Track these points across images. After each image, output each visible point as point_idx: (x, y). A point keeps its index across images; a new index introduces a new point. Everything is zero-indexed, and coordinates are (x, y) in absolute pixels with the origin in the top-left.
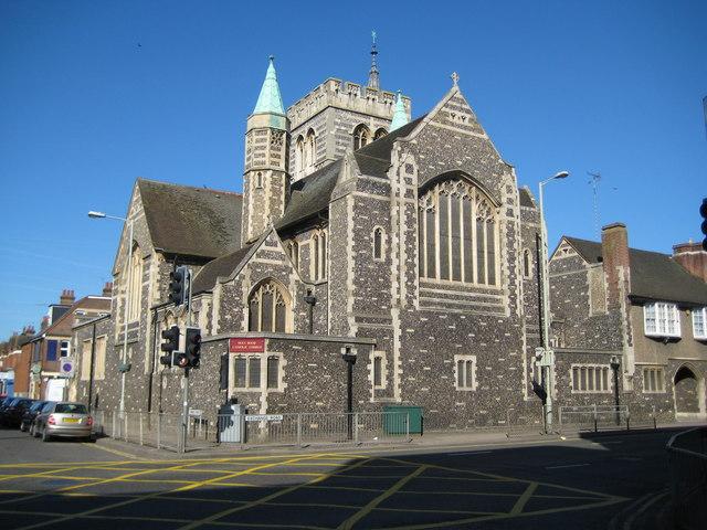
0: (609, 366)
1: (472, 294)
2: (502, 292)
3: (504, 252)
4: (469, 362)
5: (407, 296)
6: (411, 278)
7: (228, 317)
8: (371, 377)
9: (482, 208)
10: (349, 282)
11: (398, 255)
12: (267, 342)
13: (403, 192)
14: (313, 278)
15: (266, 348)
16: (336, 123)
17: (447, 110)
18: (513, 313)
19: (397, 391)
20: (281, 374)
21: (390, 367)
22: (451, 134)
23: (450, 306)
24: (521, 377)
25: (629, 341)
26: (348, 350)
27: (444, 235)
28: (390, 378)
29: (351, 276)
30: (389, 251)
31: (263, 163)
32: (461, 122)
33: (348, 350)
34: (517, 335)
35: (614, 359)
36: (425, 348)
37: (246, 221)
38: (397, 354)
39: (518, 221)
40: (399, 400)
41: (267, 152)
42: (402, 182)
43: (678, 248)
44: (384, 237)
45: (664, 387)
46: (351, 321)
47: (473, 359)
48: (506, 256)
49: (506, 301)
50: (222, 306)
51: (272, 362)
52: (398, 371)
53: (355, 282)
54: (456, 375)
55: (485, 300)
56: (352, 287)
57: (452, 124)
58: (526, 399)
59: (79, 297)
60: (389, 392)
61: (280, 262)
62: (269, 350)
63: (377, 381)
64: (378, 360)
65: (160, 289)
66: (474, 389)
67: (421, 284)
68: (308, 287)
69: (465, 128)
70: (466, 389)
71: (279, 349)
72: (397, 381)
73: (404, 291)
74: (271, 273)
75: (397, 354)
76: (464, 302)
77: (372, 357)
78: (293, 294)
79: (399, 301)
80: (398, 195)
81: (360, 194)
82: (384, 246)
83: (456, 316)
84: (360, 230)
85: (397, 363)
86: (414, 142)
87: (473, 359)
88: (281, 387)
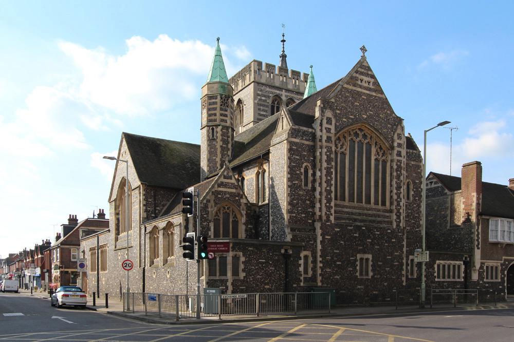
0: (462, 263)
4: (367, 260)
5: (326, 213)
6: (329, 201)
8: (301, 269)
9: (379, 150)
12: (231, 245)
13: (324, 138)
15: (231, 249)
16: (258, 95)
17: (357, 75)
18: (398, 225)
19: (319, 278)
20: (242, 266)
23: (355, 220)
24: (402, 269)
28: (314, 269)
30: (314, 181)
31: (215, 120)
32: (366, 85)
33: (286, 250)
34: (400, 240)
35: (466, 258)
38: (319, 253)
39: (404, 160)
40: (320, 284)
41: (218, 112)
42: (324, 131)
44: (310, 172)
45: (499, 277)
46: (287, 230)
47: (370, 256)
48: (395, 185)
51: (236, 259)
54: (358, 268)
55: (379, 216)
57: (361, 87)
58: (404, 284)
59: (81, 219)
61: (234, 191)
62: (233, 251)
67: (336, 205)
69: (369, 89)
71: (240, 249)
72: (319, 271)
73: (324, 209)
75: (319, 253)
77: (302, 255)
78: (244, 213)
79: (320, 216)
80: (321, 140)
82: (310, 178)
83: (359, 227)
86: (333, 100)
87: (370, 256)
88: (242, 275)
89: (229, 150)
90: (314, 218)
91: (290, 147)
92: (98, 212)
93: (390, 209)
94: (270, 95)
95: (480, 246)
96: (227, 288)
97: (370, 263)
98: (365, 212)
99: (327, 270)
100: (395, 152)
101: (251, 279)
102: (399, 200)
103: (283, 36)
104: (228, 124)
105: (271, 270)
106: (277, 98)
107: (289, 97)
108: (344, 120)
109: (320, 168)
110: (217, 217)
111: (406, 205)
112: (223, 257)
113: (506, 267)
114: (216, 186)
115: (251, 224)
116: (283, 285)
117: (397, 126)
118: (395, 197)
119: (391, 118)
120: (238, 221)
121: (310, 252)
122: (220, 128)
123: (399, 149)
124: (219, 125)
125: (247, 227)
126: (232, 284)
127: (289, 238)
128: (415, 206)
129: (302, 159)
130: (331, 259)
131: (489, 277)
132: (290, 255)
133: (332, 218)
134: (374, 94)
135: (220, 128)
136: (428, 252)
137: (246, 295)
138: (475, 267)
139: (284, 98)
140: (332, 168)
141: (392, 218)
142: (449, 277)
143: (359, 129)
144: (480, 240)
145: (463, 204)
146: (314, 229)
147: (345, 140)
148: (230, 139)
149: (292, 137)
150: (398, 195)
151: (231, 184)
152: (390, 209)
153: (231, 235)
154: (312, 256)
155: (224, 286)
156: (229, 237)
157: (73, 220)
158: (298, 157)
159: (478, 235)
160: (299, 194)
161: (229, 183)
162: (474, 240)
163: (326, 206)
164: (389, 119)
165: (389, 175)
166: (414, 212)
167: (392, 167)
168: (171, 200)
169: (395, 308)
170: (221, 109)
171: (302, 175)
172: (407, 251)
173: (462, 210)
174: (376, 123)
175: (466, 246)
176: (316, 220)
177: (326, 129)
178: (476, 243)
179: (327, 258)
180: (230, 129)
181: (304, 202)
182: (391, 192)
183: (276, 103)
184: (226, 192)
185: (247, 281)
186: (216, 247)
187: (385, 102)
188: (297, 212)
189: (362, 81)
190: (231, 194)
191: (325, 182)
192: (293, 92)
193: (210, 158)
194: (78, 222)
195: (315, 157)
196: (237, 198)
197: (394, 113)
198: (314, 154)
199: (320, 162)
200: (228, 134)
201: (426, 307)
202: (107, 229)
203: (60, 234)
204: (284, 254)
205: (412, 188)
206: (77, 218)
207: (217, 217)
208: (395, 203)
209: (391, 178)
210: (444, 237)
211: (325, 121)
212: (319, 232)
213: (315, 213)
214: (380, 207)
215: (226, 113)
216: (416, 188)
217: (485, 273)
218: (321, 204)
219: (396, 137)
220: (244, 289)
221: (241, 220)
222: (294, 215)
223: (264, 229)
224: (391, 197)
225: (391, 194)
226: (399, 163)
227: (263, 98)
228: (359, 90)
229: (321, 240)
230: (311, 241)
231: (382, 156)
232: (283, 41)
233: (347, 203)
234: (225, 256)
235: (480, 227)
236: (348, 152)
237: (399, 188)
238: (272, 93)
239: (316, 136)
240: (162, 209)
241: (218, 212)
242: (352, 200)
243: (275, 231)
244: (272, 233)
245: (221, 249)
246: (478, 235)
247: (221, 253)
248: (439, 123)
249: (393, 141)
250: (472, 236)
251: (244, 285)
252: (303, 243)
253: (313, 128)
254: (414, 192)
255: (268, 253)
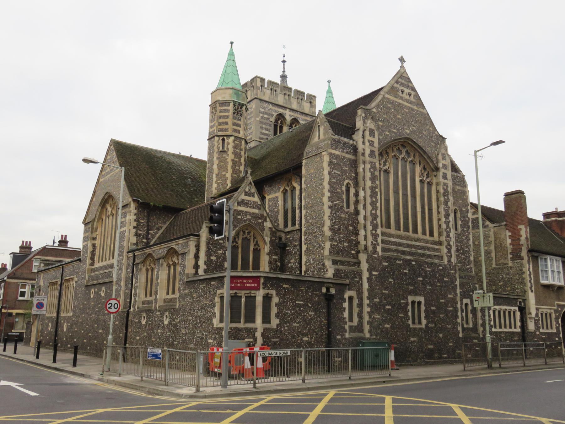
0: (517, 308)
1: (418, 244)
2: (440, 243)
3: (442, 209)
4: (419, 303)
5: (372, 243)
6: (375, 227)
7: (213, 258)
8: (346, 314)
9: (423, 171)
10: (326, 229)
11: (365, 206)
12: (262, 281)
13: (367, 152)
14: (281, 226)
15: (261, 286)
16: (260, 112)
17: (398, 86)
18: (449, 261)
19: (367, 328)
20: (274, 310)
21: (360, 305)
22: (401, 106)
23: (404, 253)
24: (457, 316)
25: (531, 288)
26: (328, 289)
27: (396, 192)
28: (360, 315)
29: (328, 223)
30: (357, 202)
31: (227, 130)
32: (407, 97)
33: (328, 289)
34: (453, 280)
35: (520, 302)
36: (386, 289)
37: (211, 180)
38: (366, 294)
39: (450, 183)
40: (368, 335)
41: (230, 121)
42: (367, 144)
43: (546, 215)
44: (352, 191)
45: (554, 327)
46: (328, 263)
47: (422, 299)
48: (443, 213)
49: (444, 250)
50: (208, 248)
51: (267, 299)
52: (367, 309)
53: (331, 229)
54: (410, 314)
55: (428, 249)
56: (328, 233)
57: (402, 98)
58: (461, 335)
59: (36, 247)
60: (359, 328)
61: (256, 211)
62: (264, 288)
63: (351, 320)
64: (351, 298)
65: (136, 235)
66: (424, 326)
68: (278, 234)
69: (411, 102)
70: (418, 326)
71: (272, 287)
72: (366, 318)
73: (370, 238)
74: (250, 220)
75: (366, 294)
76: (413, 250)
77: (346, 296)
78: (267, 239)
79: (366, 246)
80: (363, 154)
81: (334, 152)
82: (352, 199)
83: (408, 262)
84: (334, 183)
85: (366, 302)
86: (374, 110)
87: (422, 299)
88: (275, 322)
89: (242, 165)
90: (358, 249)
91: (330, 159)
92: (60, 239)
93: (439, 241)
94: (274, 113)
95: (533, 289)
96: (255, 340)
97: (423, 308)
98: (413, 243)
99: (376, 317)
100: (441, 174)
101: (286, 328)
102: (448, 230)
103: (284, 56)
104: (241, 135)
105: (311, 315)
106: (281, 117)
107: (293, 117)
108: (387, 133)
109: (363, 186)
110: (235, 244)
111: (456, 236)
112: (251, 296)
113: (559, 315)
114: (236, 204)
115: (276, 255)
116: (324, 336)
117: (440, 145)
118: (444, 226)
119: (434, 136)
120: (260, 250)
121: (355, 292)
122: (232, 139)
123: (445, 171)
124: (231, 136)
125: (271, 258)
126: (263, 334)
127: (330, 273)
128: (464, 238)
129: (343, 176)
130: (379, 302)
131: (498, 327)
132: (333, 295)
133: (379, 249)
134: (415, 107)
135: (232, 139)
136: (491, 295)
137: (289, 352)
138: (530, 313)
139: (288, 119)
140: (376, 187)
141: (442, 251)
142: (505, 327)
143: (402, 145)
144: (532, 281)
145: (509, 238)
146: (359, 264)
147: (388, 156)
148: (243, 153)
149: (332, 149)
150: (447, 223)
151: (253, 202)
152: (439, 241)
153: (251, 267)
154: (358, 298)
155: (251, 338)
156: (249, 270)
157: (26, 248)
158: (338, 173)
159: (530, 275)
160: (341, 217)
161: (250, 201)
162: (527, 280)
163: (372, 233)
164: (432, 137)
165: (436, 200)
166: (464, 245)
167: (438, 191)
168: (168, 223)
169: (460, 367)
170: (234, 118)
171: (343, 194)
172: (460, 292)
173: (508, 246)
174: (419, 139)
175: (518, 289)
176: (361, 252)
177: (369, 141)
178: (529, 285)
179: (375, 300)
180: (244, 140)
181: (346, 228)
182: (439, 220)
183: (279, 122)
184: (246, 212)
185: (281, 331)
186: (242, 283)
187: (427, 117)
188: (340, 239)
189: (403, 92)
190: (252, 214)
191: (370, 204)
192: (297, 111)
193: (219, 173)
194: (32, 250)
195: (357, 174)
196: (260, 221)
197: (436, 130)
198: (356, 170)
199: (363, 180)
200: (241, 146)
201: (493, 366)
202: (77, 258)
203: (6, 265)
204: (326, 294)
205: (459, 217)
206: (31, 246)
207: (235, 244)
208: (445, 234)
209: (437, 204)
210: (490, 277)
211: (367, 133)
212: (364, 266)
213: (359, 243)
214: (427, 237)
215: (239, 122)
216: (464, 217)
217: (540, 322)
218: (366, 231)
219: (440, 157)
220: (277, 341)
221: (264, 249)
222: (336, 243)
223: (292, 261)
224: (440, 226)
225: (438, 222)
226: (445, 187)
227: (266, 116)
228: (401, 101)
229: (368, 276)
230: (356, 278)
231: (427, 178)
232: (284, 62)
233: (392, 231)
234: (252, 295)
235: (531, 266)
236: (391, 170)
237: (447, 216)
238: (276, 112)
239: (357, 149)
240: (156, 233)
241: (237, 237)
242: (398, 228)
243: (311, 264)
244: (306, 266)
245: (249, 285)
246: (530, 275)
247: (248, 292)
248: (491, 143)
249: (438, 162)
250: (524, 276)
251: (276, 336)
252: (347, 281)
253: (353, 140)
254: (462, 221)
255: (307, 292)
